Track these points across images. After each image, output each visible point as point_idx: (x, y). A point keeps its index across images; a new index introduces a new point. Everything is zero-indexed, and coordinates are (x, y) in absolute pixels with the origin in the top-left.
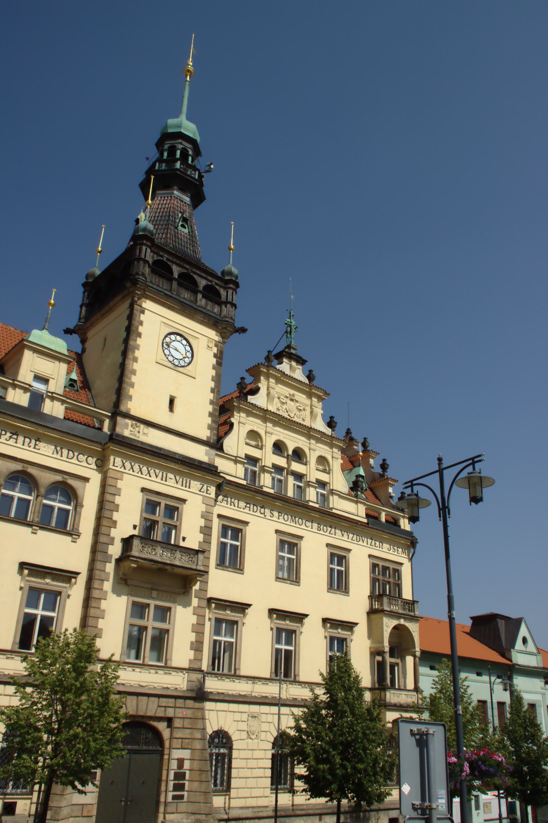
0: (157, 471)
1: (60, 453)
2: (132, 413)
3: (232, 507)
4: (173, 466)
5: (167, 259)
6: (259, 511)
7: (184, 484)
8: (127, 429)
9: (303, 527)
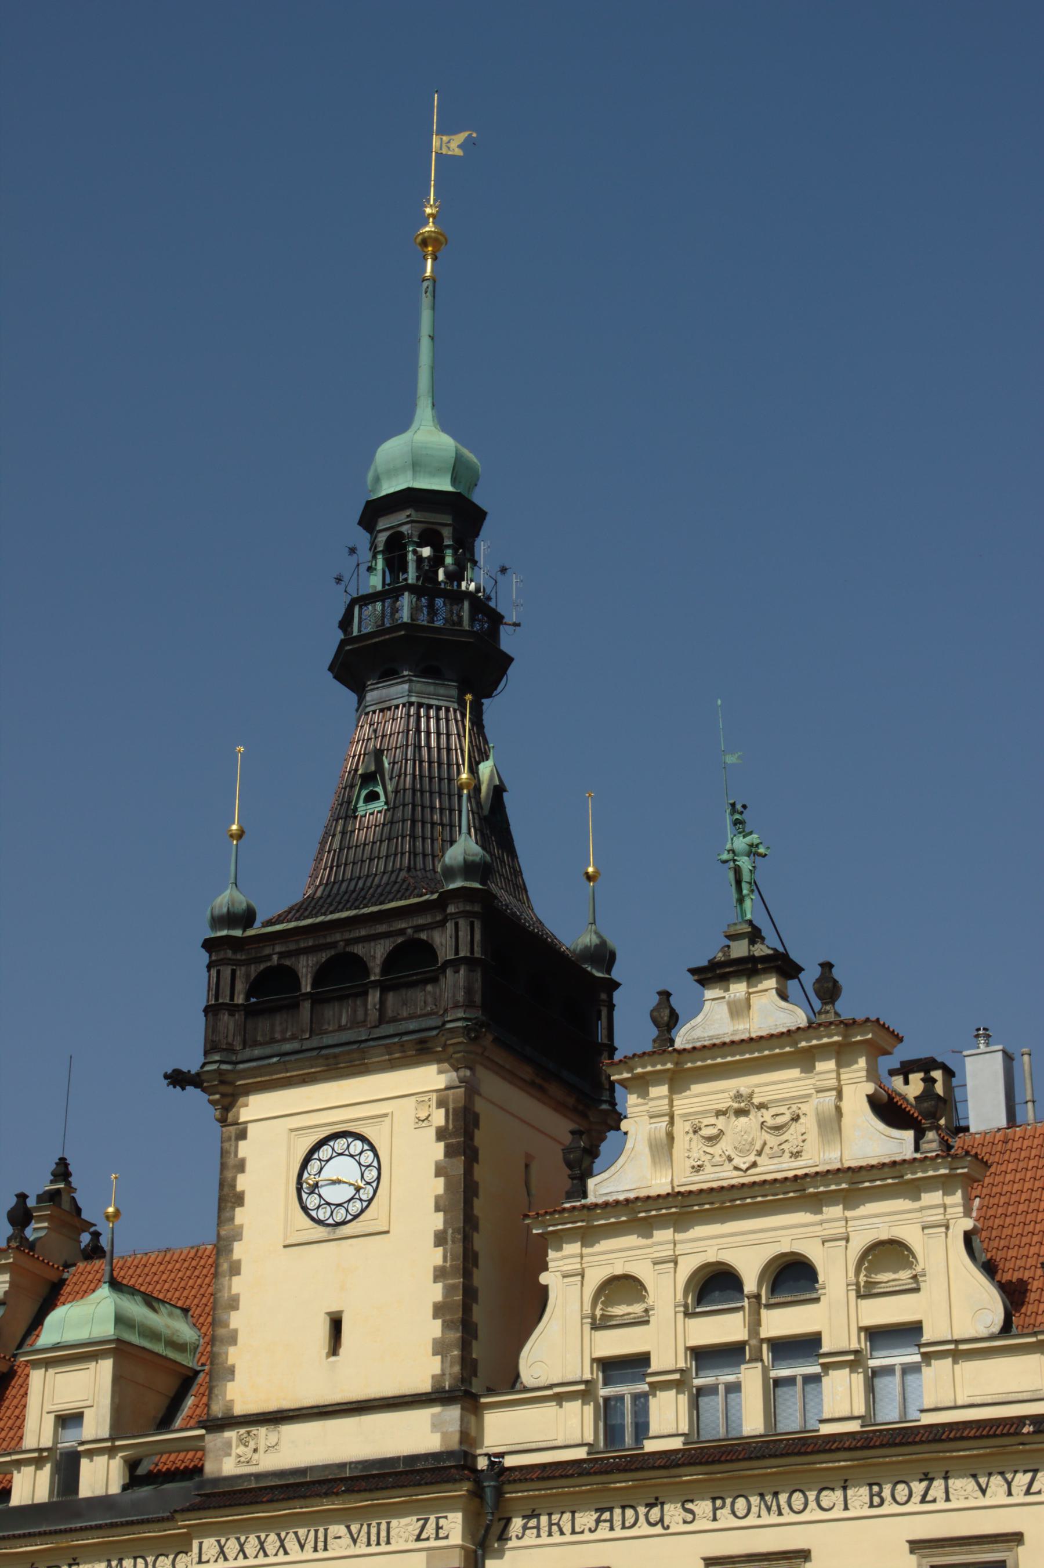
0: (302, 1532)
1: (774, 1508)
2: (239, 1410)
3: (557, 1538)
4: (328, 1505)
5: (282, 955)
6: (642, 1518)
7: (374, 1538)
8: (231, 1458)
9: (813, 1513)
